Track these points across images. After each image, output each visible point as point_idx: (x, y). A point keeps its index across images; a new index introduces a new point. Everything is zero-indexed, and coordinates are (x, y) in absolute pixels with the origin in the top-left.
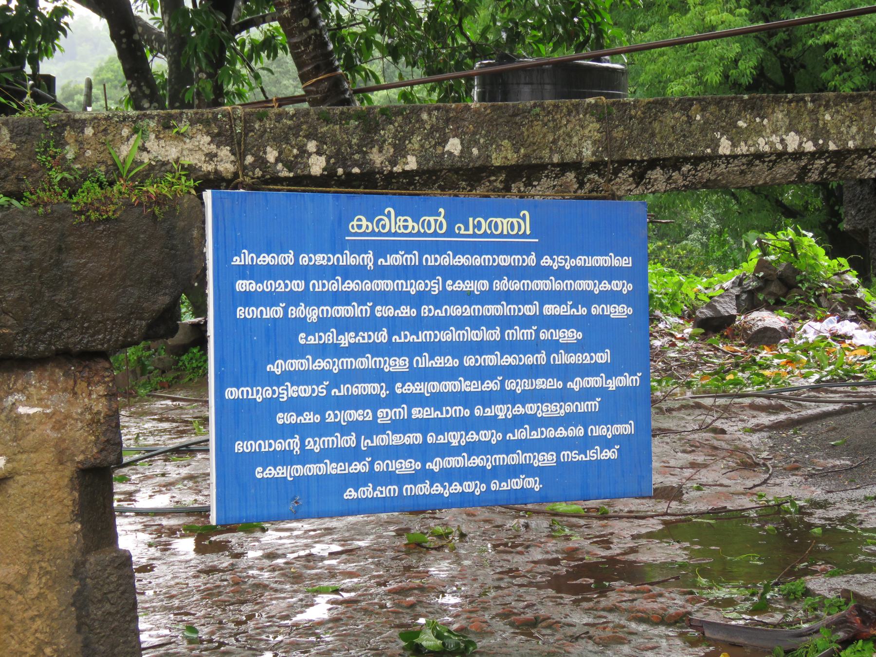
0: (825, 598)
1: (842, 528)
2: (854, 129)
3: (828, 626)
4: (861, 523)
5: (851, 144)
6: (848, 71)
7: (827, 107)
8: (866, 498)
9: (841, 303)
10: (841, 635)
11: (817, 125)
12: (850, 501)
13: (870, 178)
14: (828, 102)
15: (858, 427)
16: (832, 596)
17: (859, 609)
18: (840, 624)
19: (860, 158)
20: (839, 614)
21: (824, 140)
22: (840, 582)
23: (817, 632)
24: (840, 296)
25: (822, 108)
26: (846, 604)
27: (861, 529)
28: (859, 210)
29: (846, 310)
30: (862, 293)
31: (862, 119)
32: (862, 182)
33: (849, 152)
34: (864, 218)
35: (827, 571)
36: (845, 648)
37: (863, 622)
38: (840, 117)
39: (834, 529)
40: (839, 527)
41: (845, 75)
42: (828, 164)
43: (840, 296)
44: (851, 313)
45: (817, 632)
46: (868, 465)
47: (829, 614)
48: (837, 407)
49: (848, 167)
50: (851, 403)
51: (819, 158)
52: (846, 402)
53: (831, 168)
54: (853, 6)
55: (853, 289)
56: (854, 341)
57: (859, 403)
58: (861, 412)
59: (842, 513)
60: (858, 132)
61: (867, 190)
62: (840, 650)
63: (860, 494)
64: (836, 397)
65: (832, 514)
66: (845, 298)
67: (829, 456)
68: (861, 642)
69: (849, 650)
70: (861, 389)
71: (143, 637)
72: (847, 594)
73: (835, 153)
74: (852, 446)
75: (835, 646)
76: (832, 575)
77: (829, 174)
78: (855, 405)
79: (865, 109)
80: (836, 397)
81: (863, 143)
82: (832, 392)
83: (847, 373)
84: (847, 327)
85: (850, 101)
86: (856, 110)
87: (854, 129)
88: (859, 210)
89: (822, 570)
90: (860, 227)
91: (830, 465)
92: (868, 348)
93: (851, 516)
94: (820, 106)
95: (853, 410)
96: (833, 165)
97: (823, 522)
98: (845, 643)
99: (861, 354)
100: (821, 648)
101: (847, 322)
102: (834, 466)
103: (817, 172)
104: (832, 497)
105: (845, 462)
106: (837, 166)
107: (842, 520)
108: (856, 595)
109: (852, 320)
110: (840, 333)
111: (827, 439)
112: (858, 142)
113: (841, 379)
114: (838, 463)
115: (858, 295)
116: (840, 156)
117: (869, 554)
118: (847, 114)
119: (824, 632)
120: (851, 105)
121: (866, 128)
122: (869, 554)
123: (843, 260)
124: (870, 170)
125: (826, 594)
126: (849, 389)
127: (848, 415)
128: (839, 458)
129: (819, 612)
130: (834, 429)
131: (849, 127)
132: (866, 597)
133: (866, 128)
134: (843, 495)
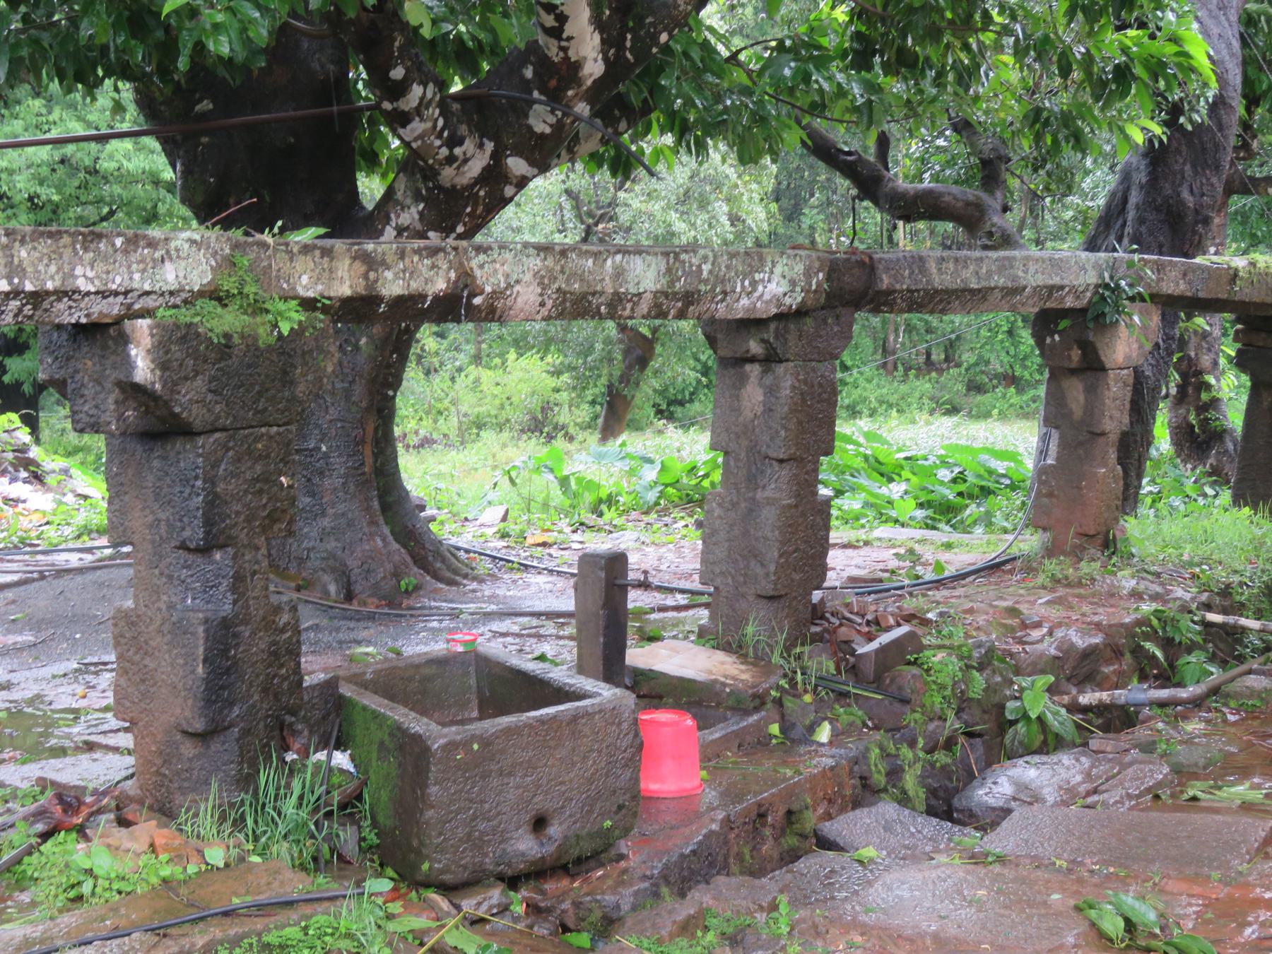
0: (17, 788)
1: (30, 710)
2: (53, 269)
3: (25, 819)
4: (50, 704)
5: (50, 286)
6: (12, 207)
7: (23, 242)
8: (54, 677)
9: (12, 464)
10: (40, 827)
11: (12, 262)
12: (36, 680)
13: (69, 324)
14: (23, 237)
15: (41, 599)
16: (25, 785)
17: (60, 797)
18: (40, 814)
19: (59, 300)
20: (36, 804)
21: (20, 279)
22: (34, 770)
23: (12, 826)
24: (10, 456)
25: (17, 244)
26: (42, 793)
27: (51, 710)
28: (57, 358)
29: (17, 470)
30: (35, 452)
31: (61, 258)
32: (59, 327)
33: (48, 293)
34: (61, 368)
35: (16, 760)
36: (45, 841)
37: (65, 811)
38: (37, 255)
39: (20, 711)
40: (26, 710)
41: (9, 212)
42: (24, 305)
43: (10, 456)
44: (24, 474)
45: (12, 826)
46: (53, 640)
47: (23, 806)
48: (15, 577)
49: (46, 310)
50: (32, 572)
51: (14, 298)
52: (25, 572)
53: (28, 310)
54: (16, 137)
55: (22, 449)
56: (27, 505)
57: (41, 572)
58: (41, 583)
59: (29, 694)
60: (57, 272)
61: (65, 336)
62: (40, 845)
63: (47, 671)
64: (14, 566)
65: (16, 695)
66: (16, 458)
67: (9, 632)
68: (63, 833)
69: (49, 843)
70: (39, 557)
71: (832, 534)
72: (43, 783)
73: (34, 295)
74: (34, 621)
75: (34, 840)
76: (23, 763)
77: (24, 316)
78: (35, 575)
79: (65, 247)
80: (14, 566)
81: (63, 284)
82: (8, 561)
83: (22, 541)
84: (20, 489)
85: (49, 237)
86: (54, 247)
87: (53, 269)
88: (57, 358)
89: (11, 758)
90: (57, 376)
91: (10, 642)
92: (44, 513)
93: (38, 697)
94: (15, 240)
95: (34, 580)
96: (29, 307)
97: (8, 705)
98: (45, 836)
99: (36, 519)
100: (17, 844)
101: (20, 484)
102: (15, 643)
103: (11, 315)
104: (15, 678)
105: (27, 637)
106: (34, 309)
107: (31, 702)
108: (53, 783)
109: (25, 481)
110: (11, 496)
111: (6, 613)
112: (58, 283)
113: (16, 547)
114: (19, 639)
115: (31, 455)
116: (37, 298)
117: (62, 737)
118: (45, 251)
119: (21, 826)
120: (49, 241)
121: (66, 268)
122: (62, 737)
123: (14, 416)
124: (70, 315)
125: (18, 784)
126: (27, 557)
127: (28, 586)
128: (21, 633)
129: (10, 805)
130: (14, 602)
131: (47, 265)
132: (535, 677)
133: (66, 268)
134: (27, 673)
